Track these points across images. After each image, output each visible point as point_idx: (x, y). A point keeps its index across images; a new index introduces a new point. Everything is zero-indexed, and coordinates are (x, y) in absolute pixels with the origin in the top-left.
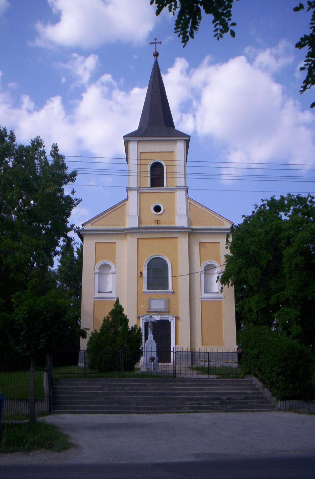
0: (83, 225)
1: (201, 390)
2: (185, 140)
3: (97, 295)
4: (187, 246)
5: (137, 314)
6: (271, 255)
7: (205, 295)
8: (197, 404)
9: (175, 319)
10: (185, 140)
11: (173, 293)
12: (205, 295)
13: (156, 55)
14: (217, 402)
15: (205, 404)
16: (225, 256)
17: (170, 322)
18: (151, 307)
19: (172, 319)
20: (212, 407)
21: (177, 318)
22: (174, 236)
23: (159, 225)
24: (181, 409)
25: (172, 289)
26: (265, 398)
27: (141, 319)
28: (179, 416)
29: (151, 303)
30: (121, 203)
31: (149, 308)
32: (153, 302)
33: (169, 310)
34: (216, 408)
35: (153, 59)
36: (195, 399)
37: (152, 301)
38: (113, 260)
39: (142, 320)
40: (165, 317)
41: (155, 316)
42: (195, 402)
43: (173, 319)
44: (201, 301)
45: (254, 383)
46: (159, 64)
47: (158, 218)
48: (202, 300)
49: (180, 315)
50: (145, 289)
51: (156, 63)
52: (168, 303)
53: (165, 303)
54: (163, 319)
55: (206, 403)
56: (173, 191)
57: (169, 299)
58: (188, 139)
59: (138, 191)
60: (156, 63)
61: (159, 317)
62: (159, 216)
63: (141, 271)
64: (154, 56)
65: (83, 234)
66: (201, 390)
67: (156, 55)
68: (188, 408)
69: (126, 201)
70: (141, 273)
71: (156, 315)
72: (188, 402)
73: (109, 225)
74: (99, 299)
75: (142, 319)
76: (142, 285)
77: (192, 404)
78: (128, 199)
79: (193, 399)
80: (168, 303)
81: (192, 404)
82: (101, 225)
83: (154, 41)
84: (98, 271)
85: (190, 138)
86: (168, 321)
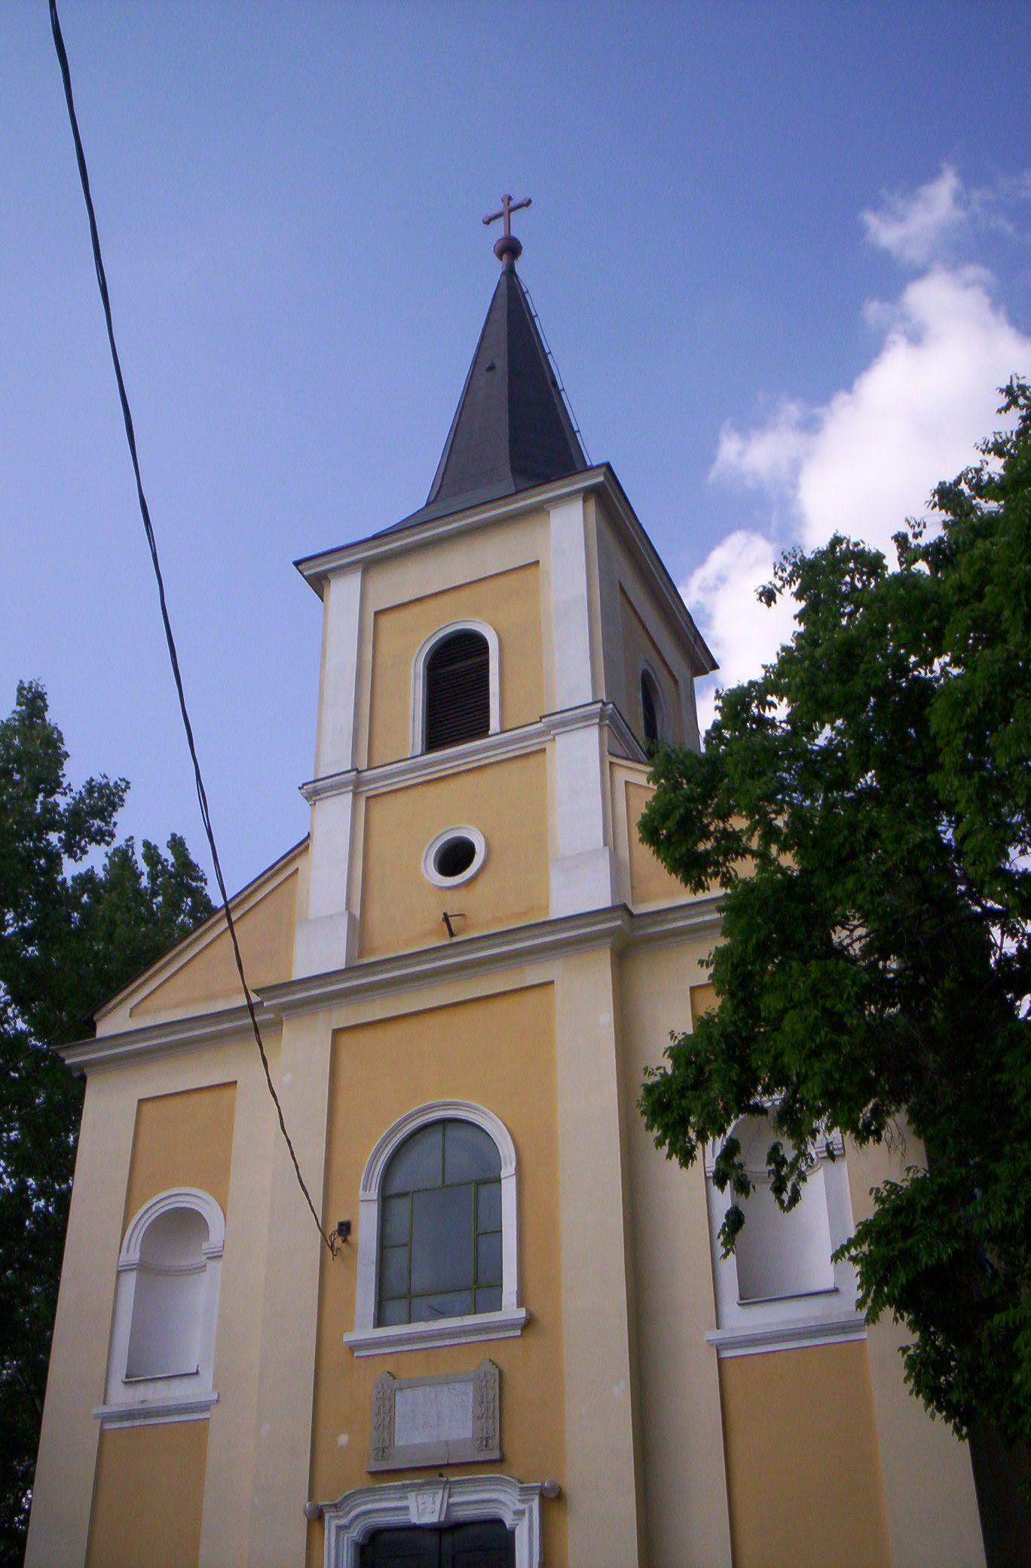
2: (588, 493)
3: (122, 1397)
4: (606, 1018)
5: (311, 1497)
6: (706, 775)
7: (742, 1320)
9: (536, 1504)
10: (588, 493)
11: (528, 1324)
12: (742, 1320)
13: (510, 249)
16: (174, 836)
17: (513, 1532)
18: (392, 1439)
19: (520, 1506)
21: (553, 1500)
22: (533, 974)
23: (455, 940)
25: (521, 1303)
27: (331, 1523)
29: (392, 1408)
30: (273, 871)
31: (383, 1450)
32: (405, 1403)
33: (501, 1449)
35: (498, 267)
37: (399, 1397)
38: (217, 1179)
39: (333, 1531)
41: (412, 1496)
44: (720, 1361)
47: (453, 904)
48: (725, 1354)
49: (571, 1483)
50: (364, 1330)
51: (510, 273)
53: (480, 1401)
54: (462, 1514)
56: (532, 745)
57: (501, 1373)
59: (356, 794)
60: (510, 273)
61: (439, 1498)
62: (463, 892)
63: (344, 1219)
64: (500, 255)
65: (80, 1066)
67: (510, 249)
69: (300, 854)
70: (345, 1229)
71: (419, 1487)
73: (212, 997)
74: (126, 1424)
75: (339, 1528)
76: (350, 1303)
78: (307, 847)
82: (178, 1005)
83: (499, 207)
86: (499, 1522)
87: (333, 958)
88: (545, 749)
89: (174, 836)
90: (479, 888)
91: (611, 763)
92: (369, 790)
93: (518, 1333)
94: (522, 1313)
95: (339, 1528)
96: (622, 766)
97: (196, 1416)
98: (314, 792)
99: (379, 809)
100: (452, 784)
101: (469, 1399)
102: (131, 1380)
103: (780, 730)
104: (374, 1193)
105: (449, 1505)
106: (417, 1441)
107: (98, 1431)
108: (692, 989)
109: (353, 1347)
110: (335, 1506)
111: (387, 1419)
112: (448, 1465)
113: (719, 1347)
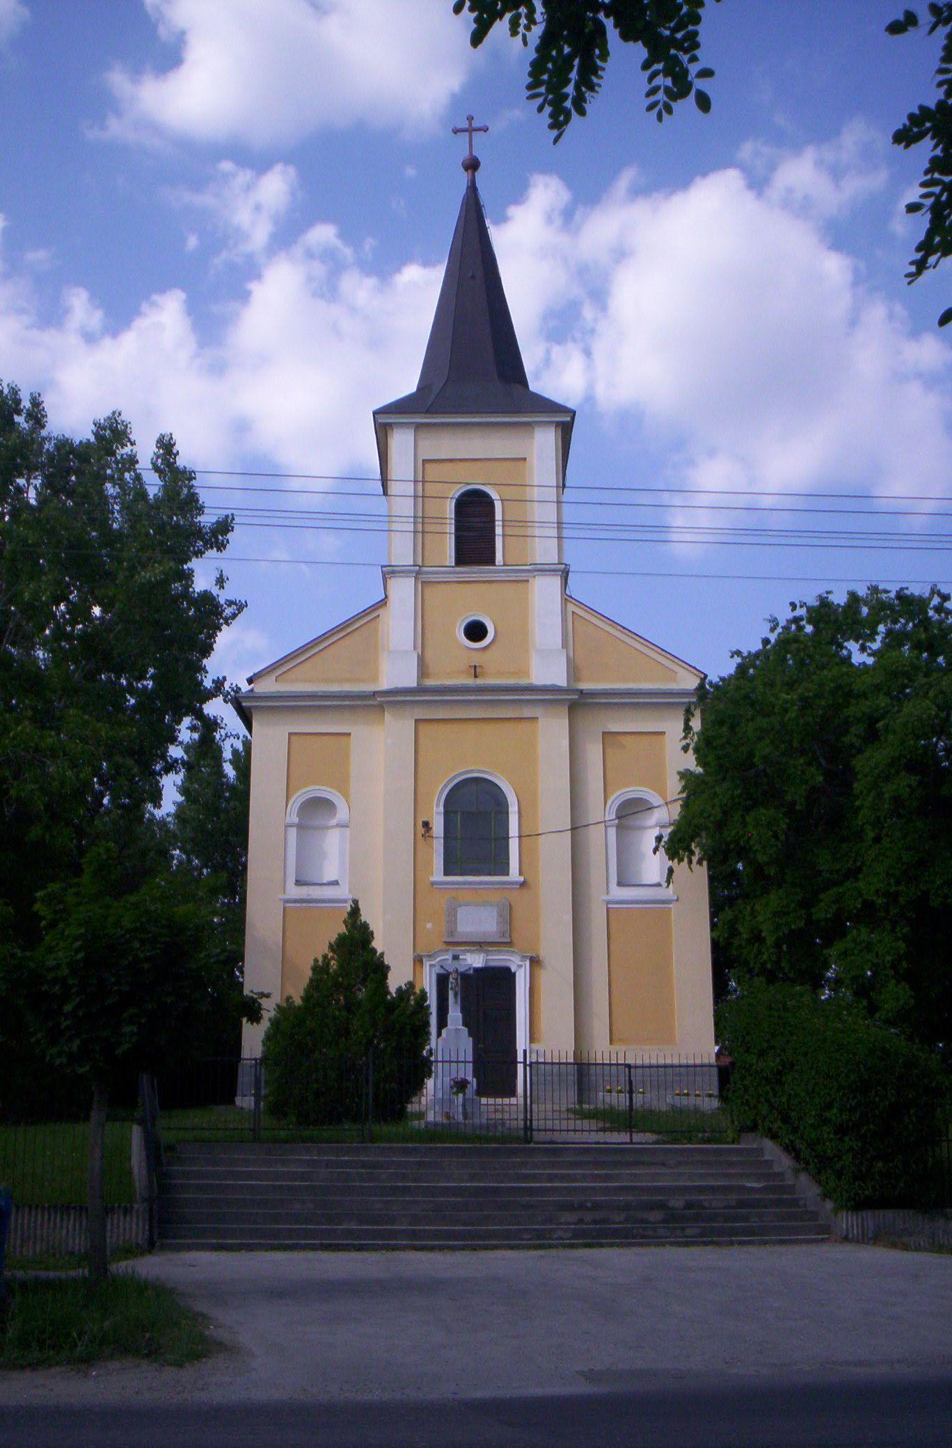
0: (250, 681)
1: (607, 1178)
2: (558, 424)
3: (294, 892)
8: (595, 1222)
9: (528, 963)
10: (558, 424)
11: (523, 885)
13: (472, 165)
14: (656, 1216)
15: (620, 1223)
16: (679, 773)
17: (514, 974)
19: (521, 963)
20: (640, 1230)
21: (535, 962)
22: (527, 712)
24: (548, 1236)
25: (521, 874)
26: (801, 1203)
27: (427, 964)
28: (542, 1256)
29: (455, 915)
30: (365, 613)
32: (462, 913)
34: (651, 1233)
35: (463, 178)
36: (589, 1205)
37: (459, 910)
38: (342, 785)
40: (499, 959)
42: (589, 1217)
43: (522, 966)
45: (767, 1157)
46: (481, 192)
47: (477, 659)
48: (610, 906)
50: (438, 875)
51: (473, 189)
52: (508, 916)
55: (622, 1219)
56: (523, 576)
58: (569, 419)
59: (416, 578)
60: (473, 189)
63: (425, 819)
65: (250, 708)
66: (607, 1178)
67: (472, 165)
68: (569, 1234)
69: (381, 607)
70: (426, 825)
71: (472, 952)
72: (568, 1217)
73: (328, 681)
76: (430, 863)
77: (581, 1221)
79: (582, 1207)
80: (508, 916)
81: (581, 1221)
82: (305, 681)
83: (465, 125)
84: (295, 820)
85: (573, 418)
86: (508, 969)
87: (409, 679)
88: (528, 581)
89: (679, 773)
90: (489, 653)
91: (566, 599)
92: (425, 578)
93: (518, 886)
94: (522, 879)
95: (431, 966)
96: (572, 603)
97: (341, 905)
98: (389, 573)
99: (428, 591)
100: (474, 586)
101: (495, 913)
102: (298, 883)
103: (755, 696)
104: (441, 809)
105: (487, 960)
106: (468, 930)
107: (282, 908)
108: (603, 733)
109: (433, 884)
110: (430, 956)
111: (453, 919)
112: (485, 942)
113: (608, 902)
